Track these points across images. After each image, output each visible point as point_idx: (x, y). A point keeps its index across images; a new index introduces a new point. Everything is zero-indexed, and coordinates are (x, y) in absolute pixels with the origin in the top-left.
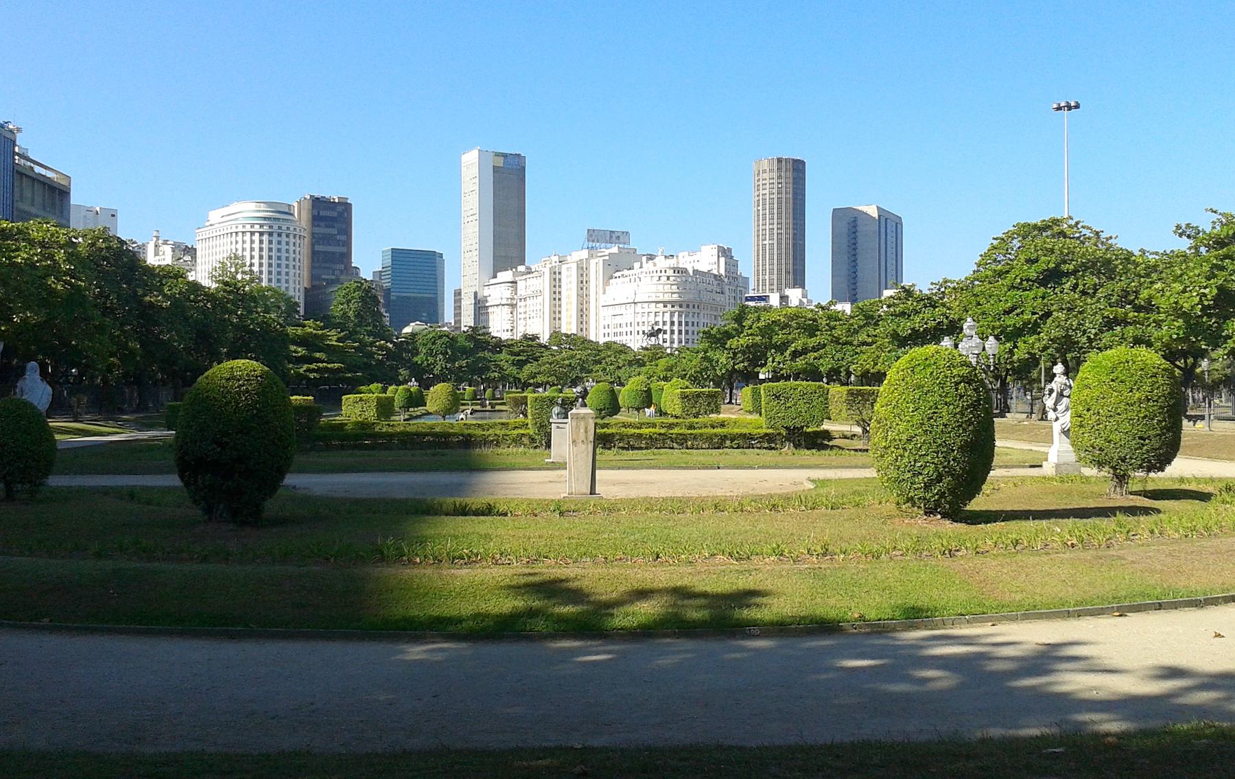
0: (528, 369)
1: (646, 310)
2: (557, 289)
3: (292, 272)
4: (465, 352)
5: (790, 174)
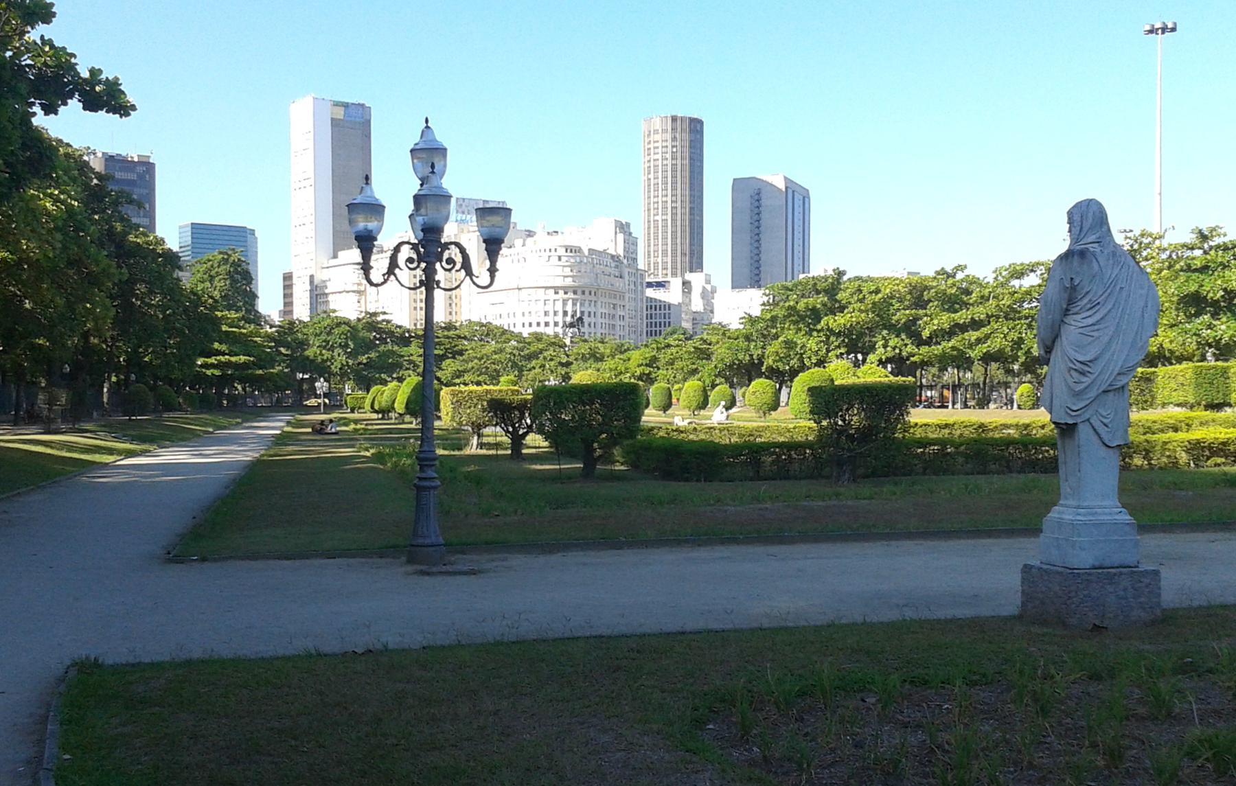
5: (686, 136)
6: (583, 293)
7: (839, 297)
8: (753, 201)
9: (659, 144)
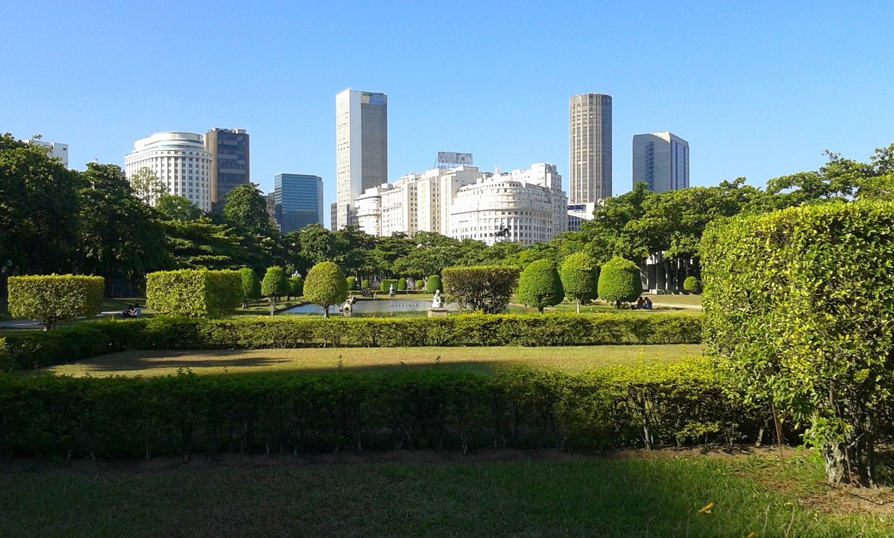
0: (398, 262)
1: (488, 217)
2: (414, 202)
3: (201, 189)
4: (342, 248)
5: (599, 108)
6: (522, 213)
7: (642, 205)
8: (648, 151)
9: (581, 114)
